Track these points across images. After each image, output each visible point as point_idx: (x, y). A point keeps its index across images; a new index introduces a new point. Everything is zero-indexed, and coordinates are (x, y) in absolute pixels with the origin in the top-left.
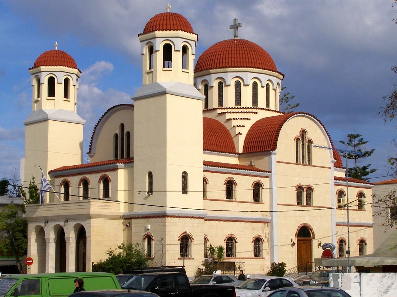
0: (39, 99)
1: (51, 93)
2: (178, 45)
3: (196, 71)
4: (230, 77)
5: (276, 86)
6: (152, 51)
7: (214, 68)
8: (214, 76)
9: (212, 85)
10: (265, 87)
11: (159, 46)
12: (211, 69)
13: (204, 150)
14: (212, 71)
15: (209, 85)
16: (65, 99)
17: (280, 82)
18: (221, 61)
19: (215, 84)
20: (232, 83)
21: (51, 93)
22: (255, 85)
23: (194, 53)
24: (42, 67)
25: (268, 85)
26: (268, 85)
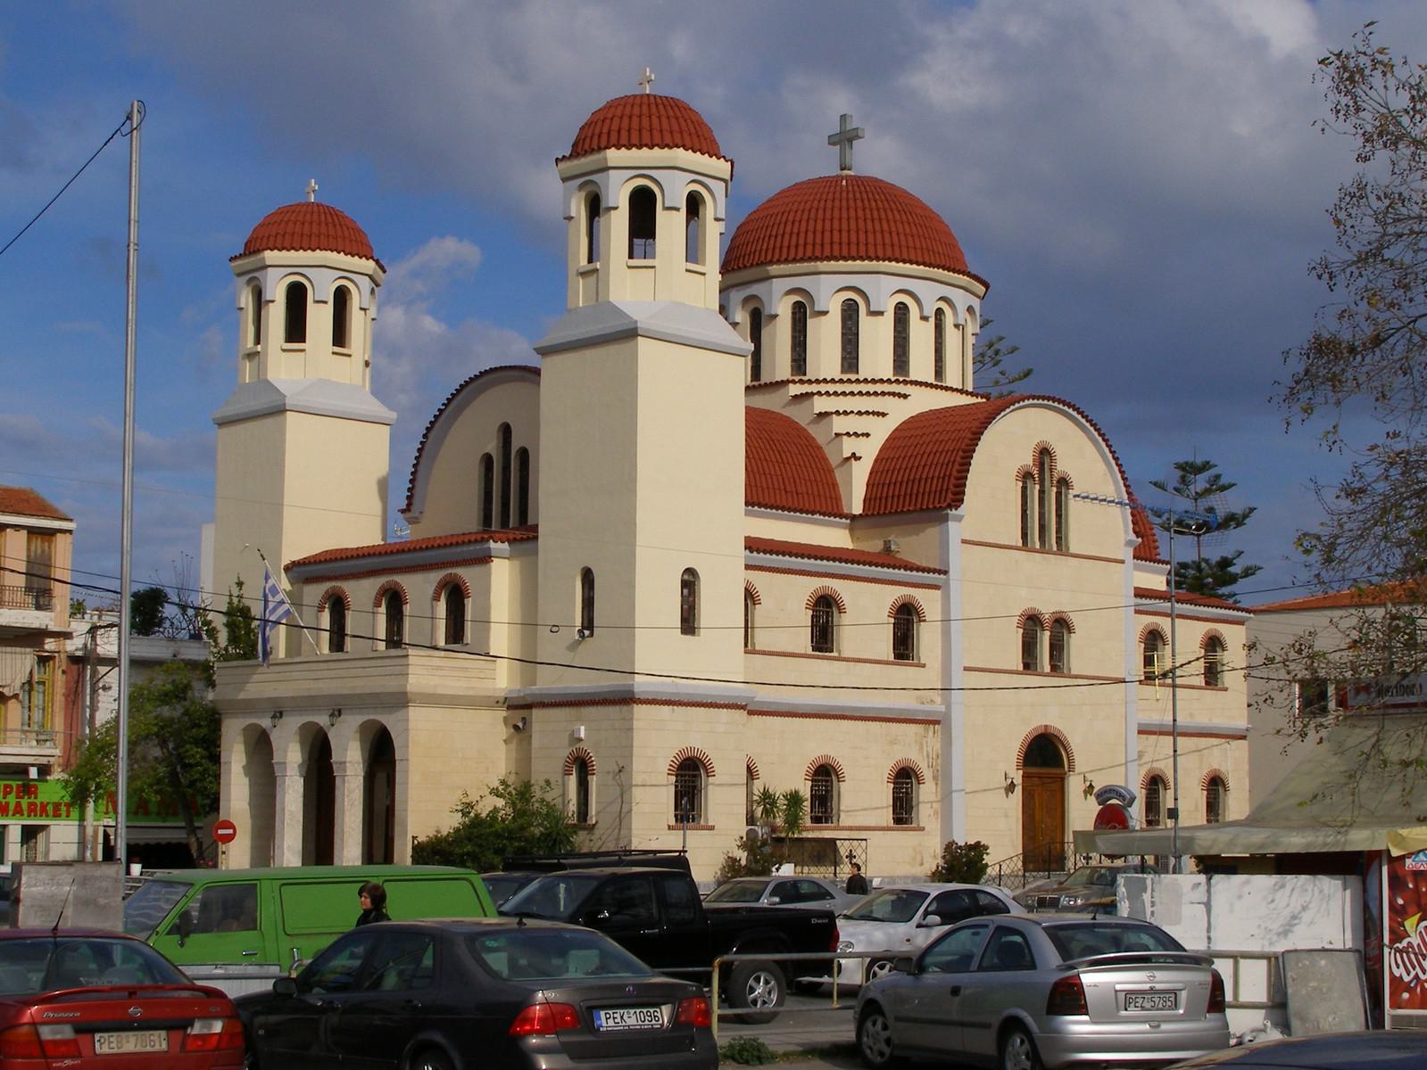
0: (259, 348)
1: (296, 330)
2: (674, 190)
3: (726, 268)
4: (828, 287)
5: (963, 316)
6: (595, 207)
7: (779, 262)
8: (780, 286)
9: (773, 313)
10: (932, 320)
11: (619, 194)
12: (771, 262)
13: (747, 504)
14: (774, 269)
15: (766, 312)
16: (337, 349)
17: (976, 303)
18: (801, 241)
19: (783, 309)
20: (835, 306)
21: (296, 330)
22: (901, 310)
23: (722, 215)
24: (268, 254)
25: (939, 312)
26: (939, 312)
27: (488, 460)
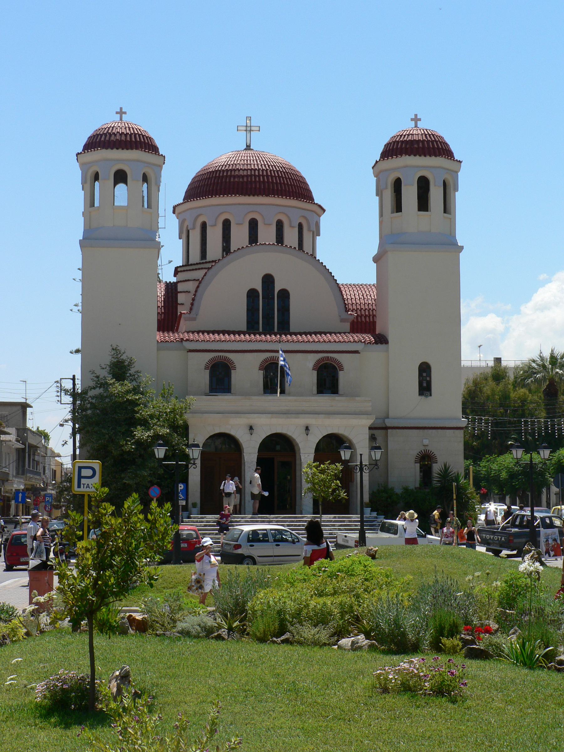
27: (252, 294)
